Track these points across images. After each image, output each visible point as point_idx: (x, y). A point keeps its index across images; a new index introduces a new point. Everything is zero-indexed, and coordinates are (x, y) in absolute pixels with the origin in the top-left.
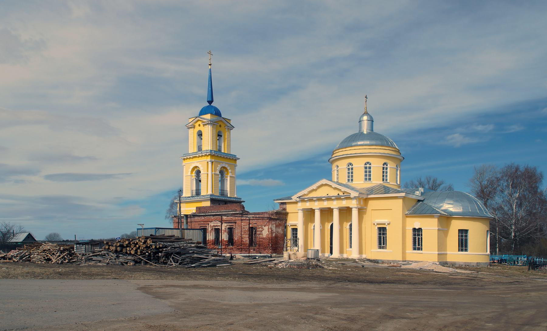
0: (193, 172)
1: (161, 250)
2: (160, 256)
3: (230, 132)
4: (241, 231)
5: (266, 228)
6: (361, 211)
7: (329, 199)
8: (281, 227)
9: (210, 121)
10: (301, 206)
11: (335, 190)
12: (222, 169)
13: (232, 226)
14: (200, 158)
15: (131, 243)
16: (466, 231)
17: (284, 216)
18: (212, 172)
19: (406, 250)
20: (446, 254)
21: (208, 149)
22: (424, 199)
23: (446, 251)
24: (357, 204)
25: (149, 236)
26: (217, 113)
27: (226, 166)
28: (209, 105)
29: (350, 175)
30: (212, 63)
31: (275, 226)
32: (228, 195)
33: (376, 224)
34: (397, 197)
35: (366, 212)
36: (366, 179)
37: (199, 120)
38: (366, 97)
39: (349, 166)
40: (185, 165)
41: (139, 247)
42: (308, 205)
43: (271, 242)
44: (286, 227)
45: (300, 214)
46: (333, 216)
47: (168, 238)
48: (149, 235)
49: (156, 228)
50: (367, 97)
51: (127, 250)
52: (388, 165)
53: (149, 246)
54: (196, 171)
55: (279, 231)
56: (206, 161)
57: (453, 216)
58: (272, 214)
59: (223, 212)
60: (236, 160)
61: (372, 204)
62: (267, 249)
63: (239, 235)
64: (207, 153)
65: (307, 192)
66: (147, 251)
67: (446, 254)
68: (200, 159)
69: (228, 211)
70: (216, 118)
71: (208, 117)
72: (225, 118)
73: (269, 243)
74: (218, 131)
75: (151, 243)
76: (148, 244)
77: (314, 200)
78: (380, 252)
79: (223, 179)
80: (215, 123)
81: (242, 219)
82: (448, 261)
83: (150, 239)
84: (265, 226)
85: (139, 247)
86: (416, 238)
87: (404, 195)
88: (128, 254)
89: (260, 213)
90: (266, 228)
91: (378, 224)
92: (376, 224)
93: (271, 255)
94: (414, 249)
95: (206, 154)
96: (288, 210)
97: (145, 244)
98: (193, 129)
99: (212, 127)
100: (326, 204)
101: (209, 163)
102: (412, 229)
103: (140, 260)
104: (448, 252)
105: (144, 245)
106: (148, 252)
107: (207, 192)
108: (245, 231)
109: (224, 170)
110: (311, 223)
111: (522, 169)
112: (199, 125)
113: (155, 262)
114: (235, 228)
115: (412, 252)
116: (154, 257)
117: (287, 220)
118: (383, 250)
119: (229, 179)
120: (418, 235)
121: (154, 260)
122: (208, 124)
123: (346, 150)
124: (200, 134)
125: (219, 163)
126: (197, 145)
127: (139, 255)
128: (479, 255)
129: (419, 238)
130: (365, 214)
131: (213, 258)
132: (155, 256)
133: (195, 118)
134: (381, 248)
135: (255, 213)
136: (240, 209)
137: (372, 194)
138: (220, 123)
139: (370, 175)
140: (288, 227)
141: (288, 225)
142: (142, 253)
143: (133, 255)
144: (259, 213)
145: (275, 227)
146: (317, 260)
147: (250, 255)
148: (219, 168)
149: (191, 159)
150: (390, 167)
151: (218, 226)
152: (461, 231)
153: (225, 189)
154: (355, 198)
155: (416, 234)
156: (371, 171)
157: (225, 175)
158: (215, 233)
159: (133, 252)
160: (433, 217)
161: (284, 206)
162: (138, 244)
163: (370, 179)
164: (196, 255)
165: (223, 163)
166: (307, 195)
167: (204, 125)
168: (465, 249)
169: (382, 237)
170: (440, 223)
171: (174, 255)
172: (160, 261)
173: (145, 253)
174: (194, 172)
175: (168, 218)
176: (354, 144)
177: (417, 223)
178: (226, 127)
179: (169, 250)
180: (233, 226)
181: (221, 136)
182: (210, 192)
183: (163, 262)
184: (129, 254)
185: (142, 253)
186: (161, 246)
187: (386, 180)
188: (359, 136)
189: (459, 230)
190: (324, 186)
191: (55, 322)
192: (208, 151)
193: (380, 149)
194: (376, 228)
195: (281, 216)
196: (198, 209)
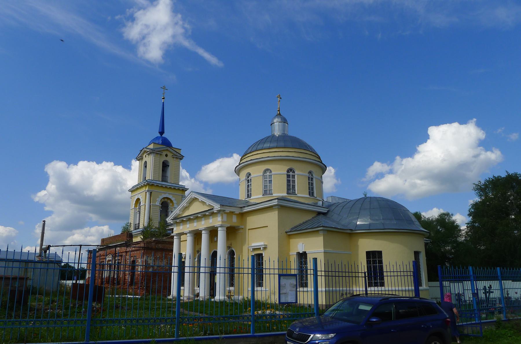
7: (196, 217)
16: (380, 253)
18: (150, 204)
22: (328, 211)
24: (222, 222)
27: (170, 197)
39: (248, 177)
56: (145, 192)
61: (252, 221)
91: (254, 249)
101: (147, 193)
109: (169, 201)
111: (429, 137)
138: (164, 153)
152: (368, 254)
160: (315, 232)
168: (375, 282)
188: (272, 138)
191: (492, 300)
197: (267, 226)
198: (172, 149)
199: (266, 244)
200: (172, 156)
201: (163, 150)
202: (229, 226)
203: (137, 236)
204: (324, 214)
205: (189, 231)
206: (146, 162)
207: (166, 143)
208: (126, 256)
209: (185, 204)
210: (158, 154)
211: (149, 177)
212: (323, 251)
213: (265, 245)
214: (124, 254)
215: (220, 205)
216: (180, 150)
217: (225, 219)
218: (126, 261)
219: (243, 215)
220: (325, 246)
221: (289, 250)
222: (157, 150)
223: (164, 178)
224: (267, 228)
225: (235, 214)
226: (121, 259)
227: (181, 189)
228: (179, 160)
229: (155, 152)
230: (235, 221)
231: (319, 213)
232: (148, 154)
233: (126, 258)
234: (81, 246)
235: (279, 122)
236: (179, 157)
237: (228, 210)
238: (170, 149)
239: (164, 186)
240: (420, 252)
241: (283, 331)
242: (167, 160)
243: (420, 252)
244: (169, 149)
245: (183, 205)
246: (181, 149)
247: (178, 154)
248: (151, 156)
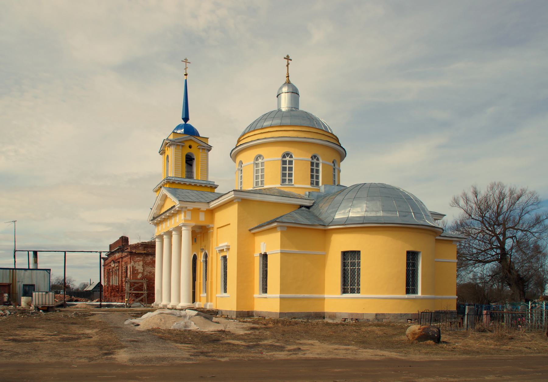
16: (356, 254)
19: (254, 293)
20: (324, 299)
21: (266, 179)
22: (314, 203)
23: (323, 292)
24: (185, 220)
28: (184, 123)
30: (188, 73)
31: (141, 263)
35: (213, 232)
38: (288, 58)
50: (187, 59)
52: (293, 157)
67: (324, 299)
82: (326, 311)
87: (233, 196)
99: (175, 148)
104: (326, 296)
115: (260, 296)
128: (399, 301)
130: (212, 237)
138: (187, 144)
146: (293, 315)
152: (345, 254)
184: (7, 302)
187: (290, 180)
198: (196, 138)
199: (229, 244)
200: (198, 147)
201: (185, 140)
202: (194, 225)
204: (308, 207)
205: (164, 232)
206: (168, 156)
207: (190, 131)
208: (122, 262)
209: (159, 202)
210: (179, 145)
211: (171, 174)
212: (280, 251)
213: (227, 246)
214: (120, 260)
215: (179, 201)
216: (207, 139)
217: (189, 217)
218: (122, 268)
219: (211, 212)
220: (282, 245)
221: (254, 251)
222: (178, 141)
223: (190, 174)
224: (228, 226)
225: (189, 210)
226: (119, 265)
227: (209, 186)
228: (206, 151)
229: (175, 143)
230: (202, 219)
231: (301, 206)
232: (169, 147)
233: (122, 264)
234: (65, 252)
235: (286, 93)
236: (206, 148)
237: (191, 206)
238: (194, 138)
240: (420, 252)
243: (420, 252)
244: (192, 138)
246: (208, 138)
247: (203, 144)
248: (171, 147)
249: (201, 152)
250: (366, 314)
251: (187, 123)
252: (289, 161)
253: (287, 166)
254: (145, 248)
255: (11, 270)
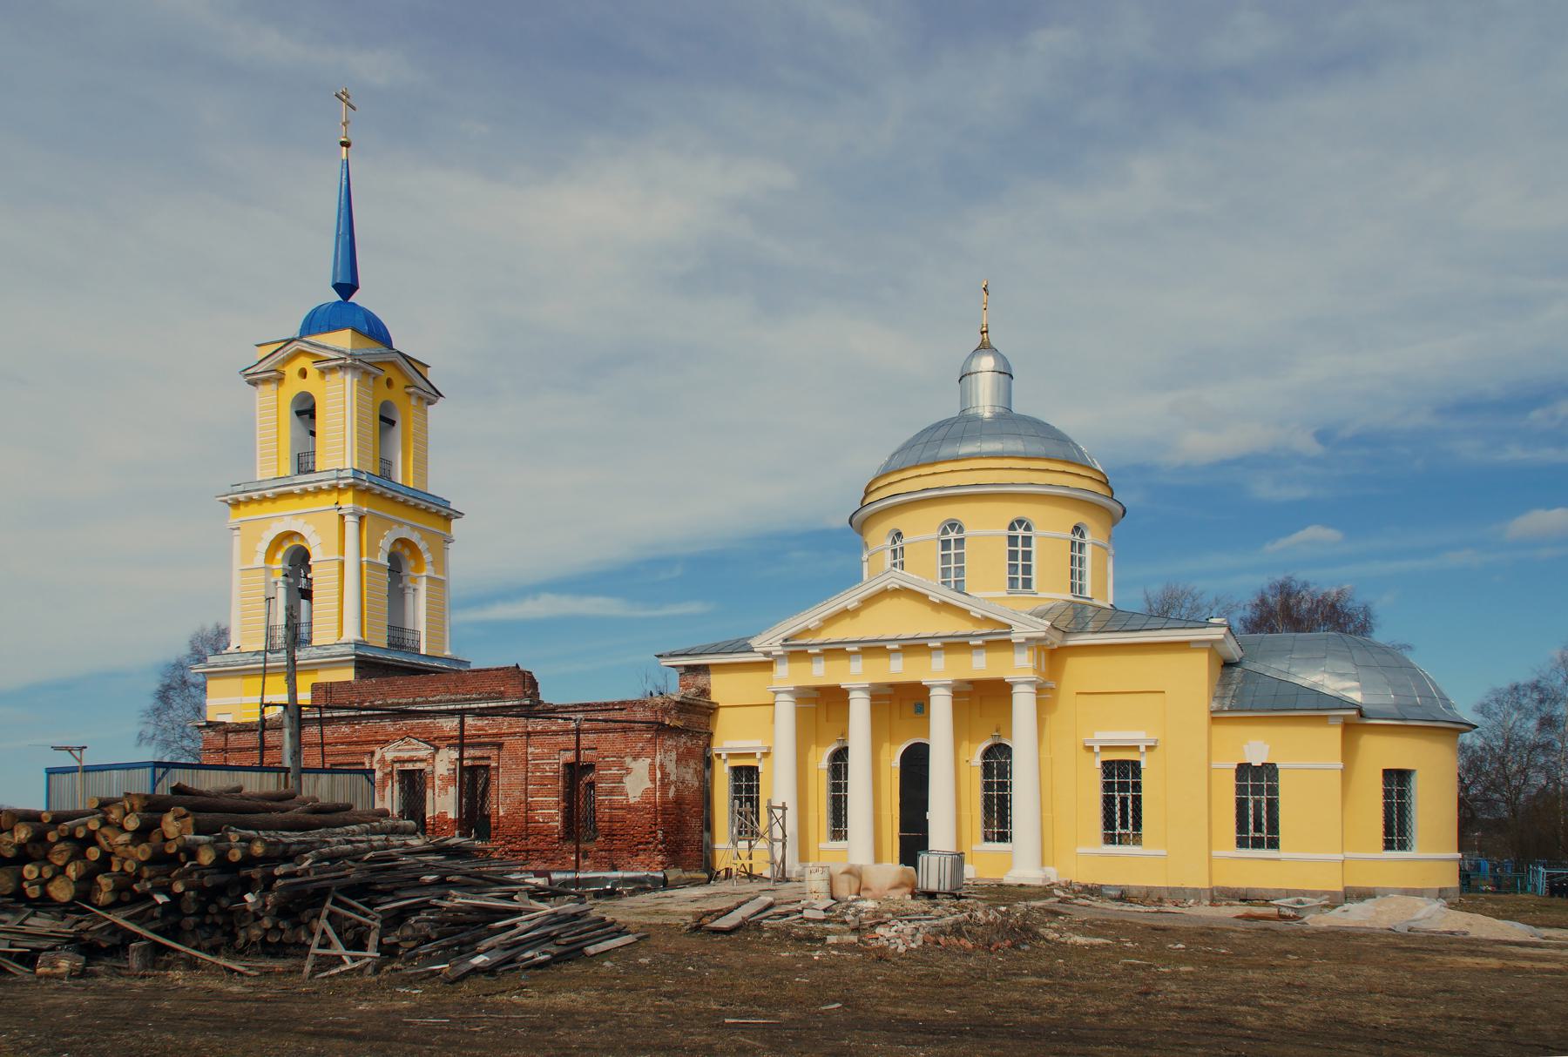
0: (274, 556)
1: (256, 873)
2: (251, 909)
3: (425, 412)
4: (526, 779)
5: (641, 767)
6: (1045, 694)
7: (914, 647)
8: (692, 763)
9: (351, 355)
10: (788, 676)
11: (939, 612)
12: (399, 547)
13: (482, 758)
14: (309, 499)
15: (52, 836)
17: (704, 719)
25: (167, 798)
26: (375, 331)
27: (415, 537)
29: (1020, 548)
31: (674, 755)
32: (419, 650)
33: (1097, 749)
34: (1187, 643)
36: (1013, 582)
37: (301, 353)
40: (238, 528)
41: (106, 859)
42: (819, 673)
43: (664, 821)
44: (708, 763)
45: (786, 711)
46: (928, 717)
47: (269, 804)
48: (122, 795)
49: (158, 765)
51: (22, 879)
52: (1088, 537)
53: (172, 850)
54: (293, 546)
55: (688, 777)
57: (1370, 718)
58: (665, 711)
59: (440, 702)
60: (448, 518)
62: (645, 850)
63: (518, 793)
64: (339, 478)
65: (819, 620)
66: (158, 880)
68: (310, 504)
69: (466, 700)
70: (371, 348)
71: (342, 340)
72: (409, 357)
73: (655, 825)
74: (380, 401)
75: (190, 837)
76: (166, 840)
77: (810, 654)
78: (1117, 855)
79: (400, 586)
80: (371, 369)
81: (530, 729)
83: (183, 811)
84: (636, 757)
85: (106, 859)
86: (1113, 797)
88: (30, 902)
89: (613, 704)
90: (641, 767)
92: (1097, 749)
93: (665, 876)
94: (1110, 839)
95: (335, 482)
96: (715, 697)
97: (147, 841)
98: (272, 387)
99: (358, 381)
100: (898, 670)
101: (348, 518)
102: (1236, 767)
103: (117, 940)
105: (144, 846)
106: (167, 890)
107: (341, 633)
108: (541, 777)
109: (407, 552)
110: (817, 744)
112: (303, 373)
113: (206, 944)
114: (498, 768)
116: (202, 912)
117: (712, 734)
118: (1121, 847)
119: (423, 587)
120: (1257, 790)
121: (201, 934)
122: (340, 367)
123: (934, 474)
124: (306, 411)
125: (389, 523)
126: (292, 451)
127: (107, 908)
129: (1124, 801)
131: (546, 908)
132: (213, 909)
133: (283, 344)
134: (1114, 843)
135: (588, 705)
136: (521, 688)
137: (1082, 631)
138: (390, 372)
139: (1027, 569)
140: (718, 764)
141: (719, 756)
142: (126, 895)
143: (65, 909)
144: (606, 704)
145: (673, 763)
147: (581, 875)
148: (385, 544)
149: (267, 505)
150: (1093, 544)
151: (416, 761)
153: (409, 626)
154: (1031, 643)
155: (1113, 783)
156: (964, 567)
157: (408, 568)
158: (402, 789)
159: (62, 891)
161: (701, 680)
162: (96, 843)
163: (1027, 584)
164: (459, 900)
165: (401, 524)
166: (818, 630)
167: (323, 372)
169: (1117, 801)
170: (122, 813)
171: (336, 902)
172: (242, 934)
173: (147, 897)
174: (280, 555)
175: (149, 744)
176: (946, 451)
177: (1257, 746)
178: (412, 390)
179: (306, 871)
180: (489, 758)
181: (392, 423)
182: (351, 634)
183: (264, 942)
185: (126, 895)
186: (258, 849)
188: (963, 426)
189: (1384, 771)
190: (891, 598)
192: (342, 474)
193: (1064, 472)
194: (1099, 765)
195: (695, 718)
196: (321, 693)
197: (1164, 692)
198: (413, 367)
203: (317, 670)
236: (429, 396)
239: (310, 487)
241: (200, 951)
242: (387, 401)
243: (1414, 771)
245: (885, 583)
248: (345, 374)
249: (414, 406)
250: (1427, 889)
251: (349, 301)
252: (1023, 537)
253: (1020, 548)
254: (680, 711)
255: (283, 775)
